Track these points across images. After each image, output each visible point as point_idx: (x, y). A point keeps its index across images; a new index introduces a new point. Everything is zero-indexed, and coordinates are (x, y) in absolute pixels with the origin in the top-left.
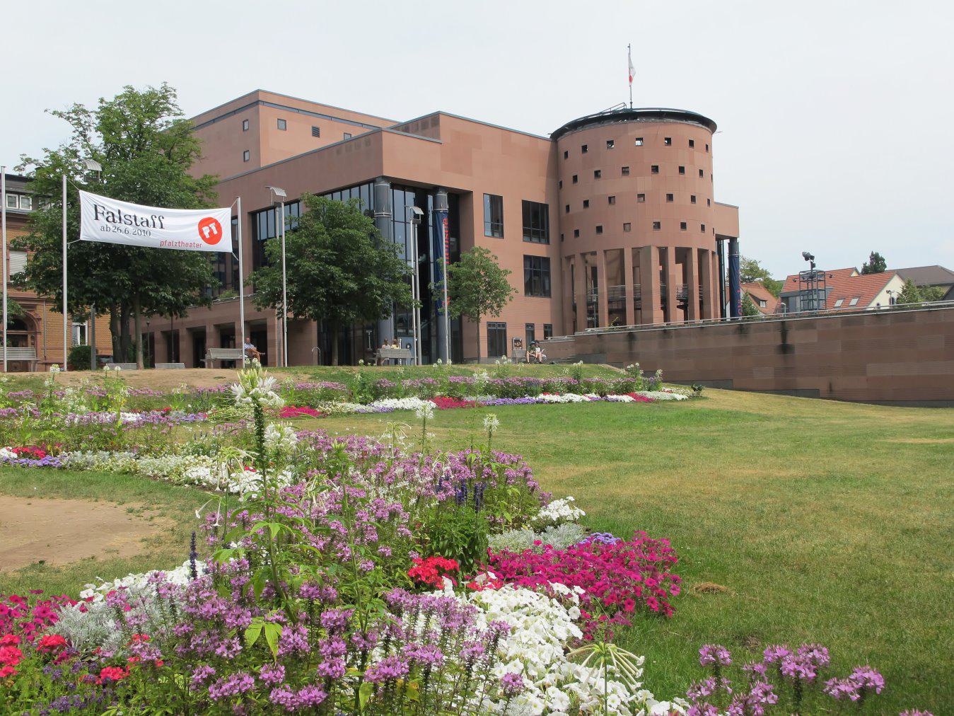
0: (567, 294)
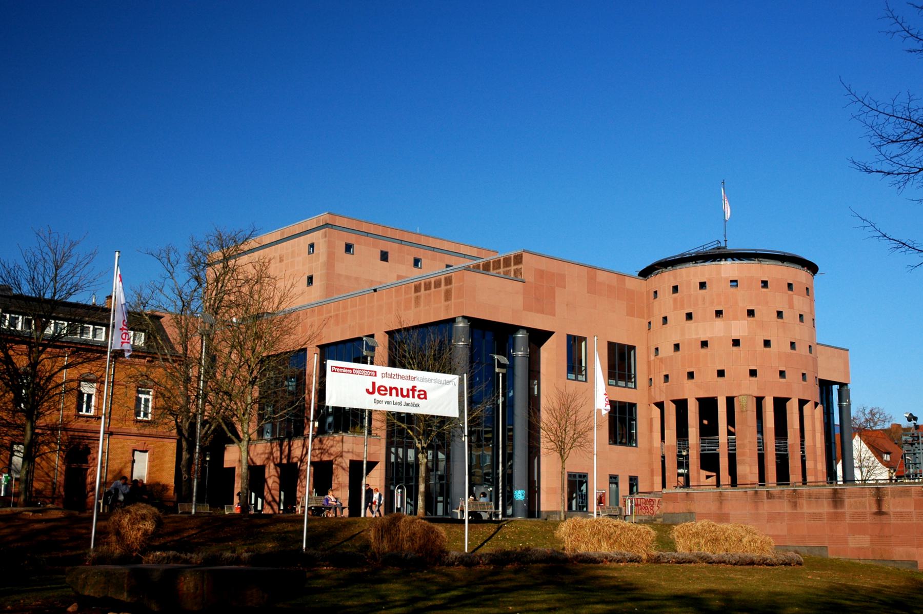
0: (821, 484)
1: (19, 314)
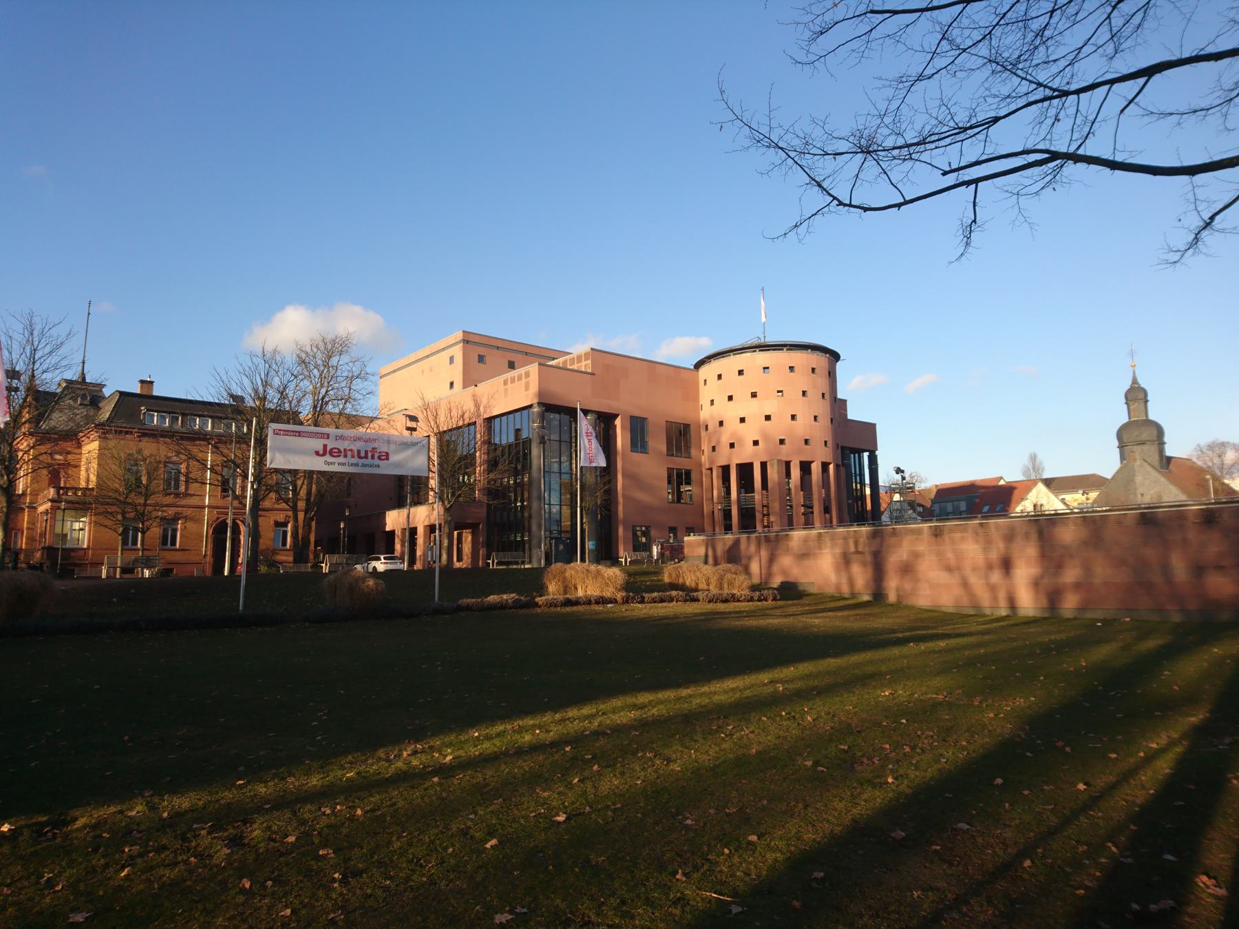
1: (156, 411)
